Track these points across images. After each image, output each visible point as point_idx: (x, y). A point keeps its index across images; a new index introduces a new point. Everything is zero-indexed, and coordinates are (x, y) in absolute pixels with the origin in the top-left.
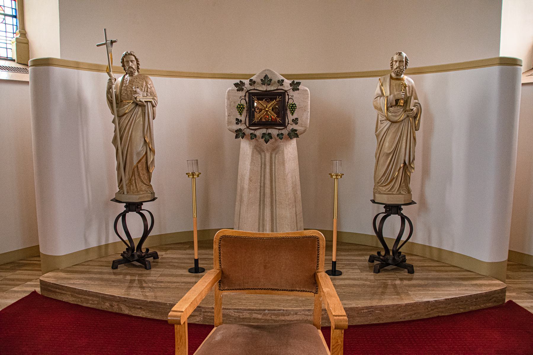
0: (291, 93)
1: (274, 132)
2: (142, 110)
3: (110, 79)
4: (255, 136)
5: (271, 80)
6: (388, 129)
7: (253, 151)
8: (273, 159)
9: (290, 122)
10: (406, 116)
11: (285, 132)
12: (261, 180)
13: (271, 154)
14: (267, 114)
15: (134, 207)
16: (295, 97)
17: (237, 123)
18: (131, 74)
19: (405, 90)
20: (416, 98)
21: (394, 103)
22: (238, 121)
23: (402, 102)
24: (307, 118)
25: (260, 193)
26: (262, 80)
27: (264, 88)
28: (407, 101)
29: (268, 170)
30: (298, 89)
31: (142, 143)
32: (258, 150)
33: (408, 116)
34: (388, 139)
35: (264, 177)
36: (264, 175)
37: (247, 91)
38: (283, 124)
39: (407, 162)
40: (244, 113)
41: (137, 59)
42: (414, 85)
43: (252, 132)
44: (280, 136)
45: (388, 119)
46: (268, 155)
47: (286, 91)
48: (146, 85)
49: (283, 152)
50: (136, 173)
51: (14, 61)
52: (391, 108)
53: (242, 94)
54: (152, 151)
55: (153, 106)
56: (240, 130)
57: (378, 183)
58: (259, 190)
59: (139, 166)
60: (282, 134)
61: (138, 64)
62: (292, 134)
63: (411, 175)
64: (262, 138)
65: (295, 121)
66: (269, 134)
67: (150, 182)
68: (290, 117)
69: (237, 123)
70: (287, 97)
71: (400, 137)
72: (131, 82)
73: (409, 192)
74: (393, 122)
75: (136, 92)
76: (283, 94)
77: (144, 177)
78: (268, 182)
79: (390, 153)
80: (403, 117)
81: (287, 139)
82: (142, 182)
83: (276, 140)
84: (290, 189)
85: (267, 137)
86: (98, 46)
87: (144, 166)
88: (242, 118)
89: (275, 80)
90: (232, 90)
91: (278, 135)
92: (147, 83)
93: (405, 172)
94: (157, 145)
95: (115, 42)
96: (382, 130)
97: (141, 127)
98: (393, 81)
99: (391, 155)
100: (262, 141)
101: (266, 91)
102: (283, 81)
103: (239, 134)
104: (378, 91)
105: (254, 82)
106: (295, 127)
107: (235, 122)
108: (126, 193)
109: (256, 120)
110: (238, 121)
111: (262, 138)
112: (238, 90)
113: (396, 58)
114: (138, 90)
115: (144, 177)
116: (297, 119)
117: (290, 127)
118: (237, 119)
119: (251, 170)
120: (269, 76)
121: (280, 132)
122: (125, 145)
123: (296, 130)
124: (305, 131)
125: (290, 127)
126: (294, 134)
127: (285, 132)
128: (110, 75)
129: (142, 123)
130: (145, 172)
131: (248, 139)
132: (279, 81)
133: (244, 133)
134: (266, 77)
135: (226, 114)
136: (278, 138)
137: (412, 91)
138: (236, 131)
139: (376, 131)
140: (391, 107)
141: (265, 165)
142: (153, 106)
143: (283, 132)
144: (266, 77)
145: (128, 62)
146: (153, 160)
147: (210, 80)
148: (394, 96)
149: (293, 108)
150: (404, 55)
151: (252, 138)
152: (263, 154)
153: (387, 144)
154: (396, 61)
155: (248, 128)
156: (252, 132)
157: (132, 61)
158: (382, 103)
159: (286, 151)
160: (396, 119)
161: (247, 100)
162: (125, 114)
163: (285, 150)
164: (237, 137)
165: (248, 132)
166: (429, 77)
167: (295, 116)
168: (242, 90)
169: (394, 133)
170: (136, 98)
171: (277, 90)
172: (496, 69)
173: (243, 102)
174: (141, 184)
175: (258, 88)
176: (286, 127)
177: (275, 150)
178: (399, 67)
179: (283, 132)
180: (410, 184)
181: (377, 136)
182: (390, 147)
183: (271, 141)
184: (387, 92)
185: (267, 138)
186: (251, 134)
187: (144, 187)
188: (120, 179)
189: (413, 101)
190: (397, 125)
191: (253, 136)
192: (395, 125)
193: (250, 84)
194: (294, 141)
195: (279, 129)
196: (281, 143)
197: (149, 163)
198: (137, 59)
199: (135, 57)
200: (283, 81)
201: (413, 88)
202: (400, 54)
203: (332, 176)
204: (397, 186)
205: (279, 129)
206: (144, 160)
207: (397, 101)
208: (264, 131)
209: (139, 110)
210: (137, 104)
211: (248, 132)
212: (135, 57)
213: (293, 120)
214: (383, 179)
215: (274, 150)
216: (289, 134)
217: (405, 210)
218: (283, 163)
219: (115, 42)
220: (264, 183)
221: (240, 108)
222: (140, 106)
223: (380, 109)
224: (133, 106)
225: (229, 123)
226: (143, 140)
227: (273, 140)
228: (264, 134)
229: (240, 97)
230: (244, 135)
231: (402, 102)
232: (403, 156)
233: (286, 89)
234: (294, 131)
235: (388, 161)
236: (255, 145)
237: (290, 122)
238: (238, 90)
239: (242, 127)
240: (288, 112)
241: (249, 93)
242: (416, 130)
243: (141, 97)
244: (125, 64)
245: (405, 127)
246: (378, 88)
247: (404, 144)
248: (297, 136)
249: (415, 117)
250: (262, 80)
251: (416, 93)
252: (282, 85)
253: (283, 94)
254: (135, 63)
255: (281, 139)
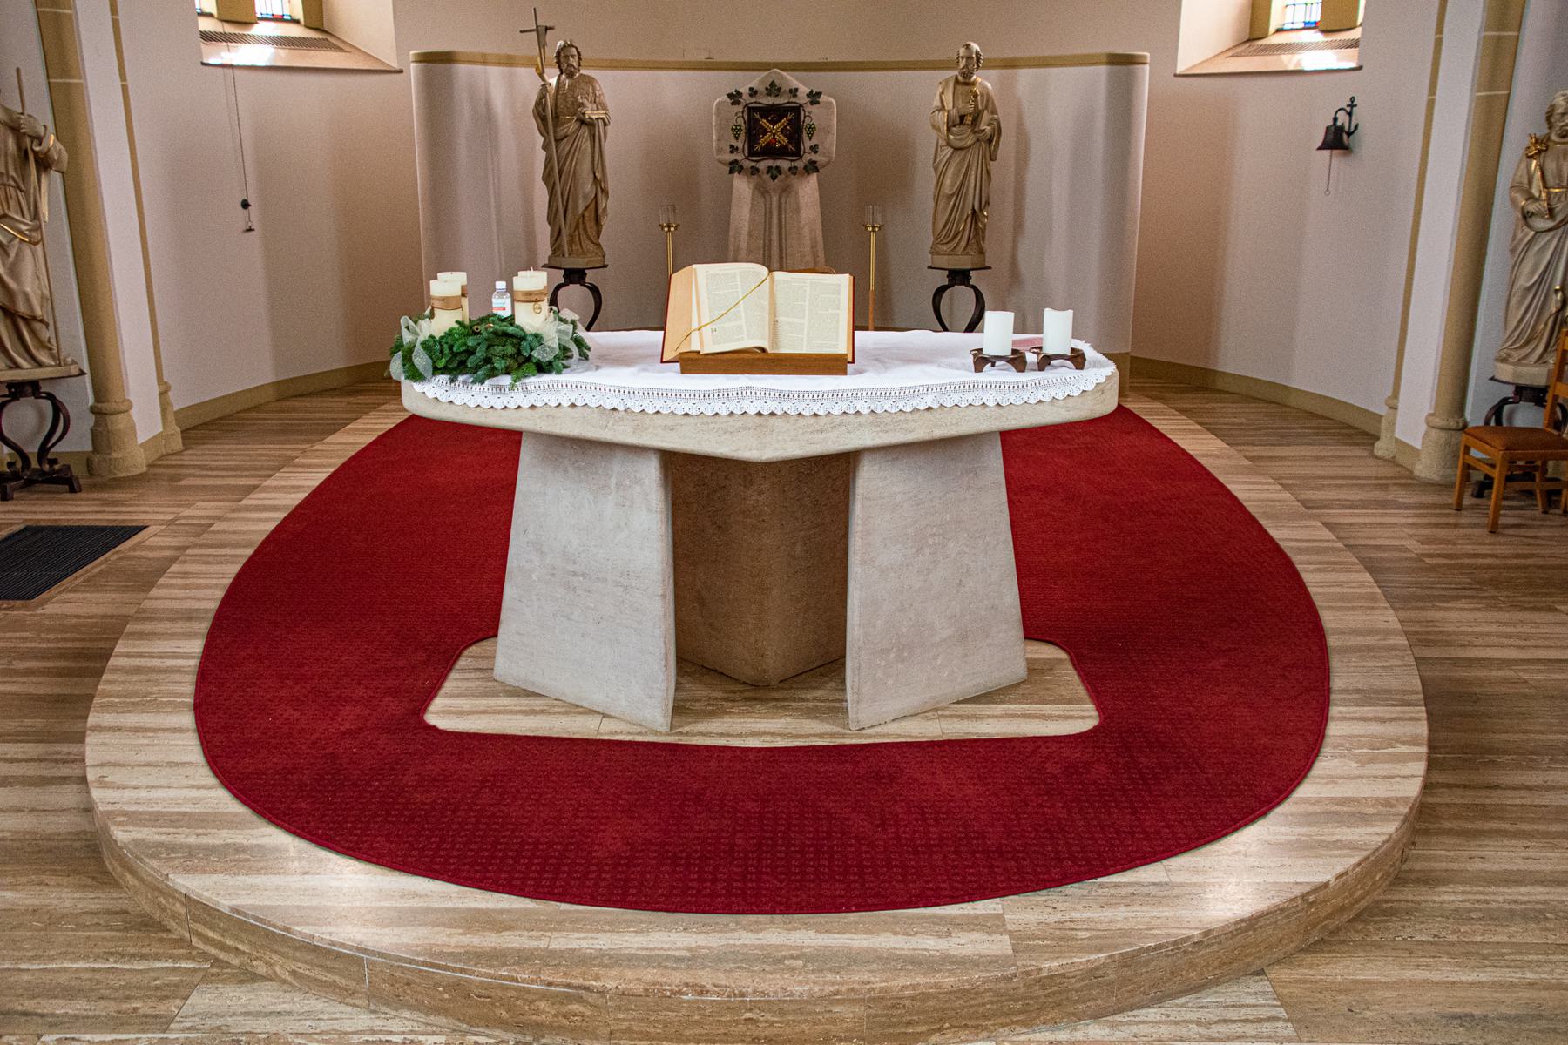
0: (808, 108)
1: (784, 164)
2: (590, 133)
3: (543, 85)
4: (758, 170)
5: (779, 89)
6: (950, 157)
7: (753, 191)
8: (783, 205)
9: (807, 150)
10: (975, 139)
11: (800, 164)
12: (764, 235)
13: (780, 198)
14: (774, 138)
15: (576, 276)
16: (813, 115)
17: (732, 152)
18: (570, 75)
19: (975, 100)
20: (994, 112)
21: (958, 121)
22: (733, 149)
23: (969, 119)
24: (832, 144)
25: (764, 254)
26: (766, 89)
27: (769, 101)
28: (976, 118)
29: (775, 220)
30: (818, 103)
31: (591, 181)
32: (761, 190)
33: (978, 140)
34: (950, 173)
35: (770, 231)
36: (770, 228)
37: (747, 105)
38: (798, 154)
39: (976, 208)
40: (742, 136)
41: (579, 53)
42: (992, 93)
43: (753, 164)
44: (793, 170)
45: (949, 144)
46: (775, 199)
47: (801, 105)
48: (594, 93)
49: (797, 193)
50: (581, 226)
51: (297, 22)
52: (954, 129)
53: (739, 108)
54: (605, 192)
55: (605, 125)
56: (736, 162)
57: (937, 239)
58: (762, 252)
59: (586, 214)
60: (796, 168)
61: (580, 59)
62: (810, 167)
63: (387, 62)
64: (768, 173)
65: (814, 149)
66: (777, 168)
67: (598, 237)
68: (807, 143)
69: (732, 152)
70: (802, 113)
71: (966, 174)
72: (572, 87)
73: (982, 252)
74: (956, 149)
75: (582, 105)
76: (797, 110)
77: (592, 232)
78: (775, 237)
79: (952, 195)
80: (970, 141)
81: (803, 175)
82: (590, 239)
83: (787, 176)
84: (807, 242)
85: (775, 172)
86: (521, 32)
87: (593, 216)
88: (739, 144)
89: (785, 88)
90: (723, 102)
91: (790, 169)
92: (594, 89)
93: (976, 223)
94: (612, 184)
95: (551, 28)
96: (941, 161)
97: (589, 158)
98: (959, 88)
99: (1531, 296)
100: (767, 177)
101: (773, 105)
102: (796, 90)
103: (735, 167)
104: (937, 103)
105: (756, 92)
106: (814, 157)
107: (729, 149)
108: (567, 255)
109: (758, 148)
110: (733, 149)
111: (768, 173)
112: (732, 104)
113: (962, 51)
114: (585, 101)
115: (592, 232)
116: (816, 145)
117: (808, 157)
118: (732, 146)
119: (752, 221)
120: (777, 82)
121: (793, 164)
122: (566, 183)
123: (815, 162)
124: (828, 163)
125: (808, 157)
126: (812, 167)
127: (800, 164)
128: (543, 79)
129: (589, 150)
130: (593, 223)
131: (747, 175)
132: (791, 91)
133: (741, 167)
134: (773, 84)
135: (714, 137)
136: (789, 173)
137: (988, 101)
138: (731, 163)
139: (935, 160)
140: (955, 126)
141: (771, 212)
142: (605, 125)
143: (796, 164)
144: (773, 84)
145: (567, 57)
146: (605, 207)
147: (675, 73)
148: (958, 111)
149: (811, 130)
150: (975, 47)
151: (752, 174)
152: (767, 196)
153: (948, 182)
154: (963, 58)
155: (747, 158)
156: (753, 164)
157: (573, 56)
158: (942, 118)
159: (801, 193)
160: (960, 144)
161: (746, 117)
162: (566, 137)
163: (800, 191)
164: (731, 172)
165: (747, 164)
166: (1025, 76)
167: (812, 143)
168: (739, 103)
169: (735, 97)
170: (584, 114)
171: (788, 103)
172: (1103, 70)
173: (740, 121)
174: (588, 242)
175: (761, 101)
176: (801, 157)
177: (786, 190)
178: (966, 66)
179: (796, 164)
180: (986, 242)
181: (936, 169)
182: (952, 185)
183: (780, 177)
184: (949, 105)
185: (774, 173)
186: (752, 167)
187: (592, 247)
188: (556, 234)
189: (986, 117)
190: (963, 152)
191: (754, 171)
192: (959, 152)
193: (751, 95)
194: (814, 177)
195: (792, 161)
196: (794, 180)
197: (600, 211)
198: (579, 53)
199: (577, 49)
200: (796, 90)
201: (988, 95)
202: (968, 47)
203: (866, 228)
204: (963, 243)
205: (792, 161)
206: (593, 206)
207: (962, 118)
208: (770, 163)
209: (585, 131)
210: (582, 122)
211: (747, 164)
212: (577, 49)
213: (811, 147)
214: (944, 233)
215: (784, 190)
216: (805, 168)
217: (975, 278)
218: (798, 210)
219: (551, 28)
220: (770, 241)
221: (736, 131)
222: (587, 124)
223: (938, 130)
224: (578, 124)
225: (719, 151)
226: (592, 176)
227: (783, 176)
228: (770, 168)
229: (737, 115)
230: (741, 170)
231: (969, 119)
232: (971, 200)
233: (801, 102)
234: (813, 162)
235: (950, 206)
236: (757, 185)
237: (807, 150)
238: (732, 104)
239: (739, 157)
240: (805, 134)
241: (749, 109)
242: (991, 160)
243: (591, 113)
244: (562, 60)
245: (975, 156)
246: (938, 97)
247: (973, 181)
248: (816, 170)
249: (990, 141)
250: (766, 89)
251: (993, 103)
252: (795, 96)
253: (797, 110)
254: (576, 58)
255: (795, 174)
